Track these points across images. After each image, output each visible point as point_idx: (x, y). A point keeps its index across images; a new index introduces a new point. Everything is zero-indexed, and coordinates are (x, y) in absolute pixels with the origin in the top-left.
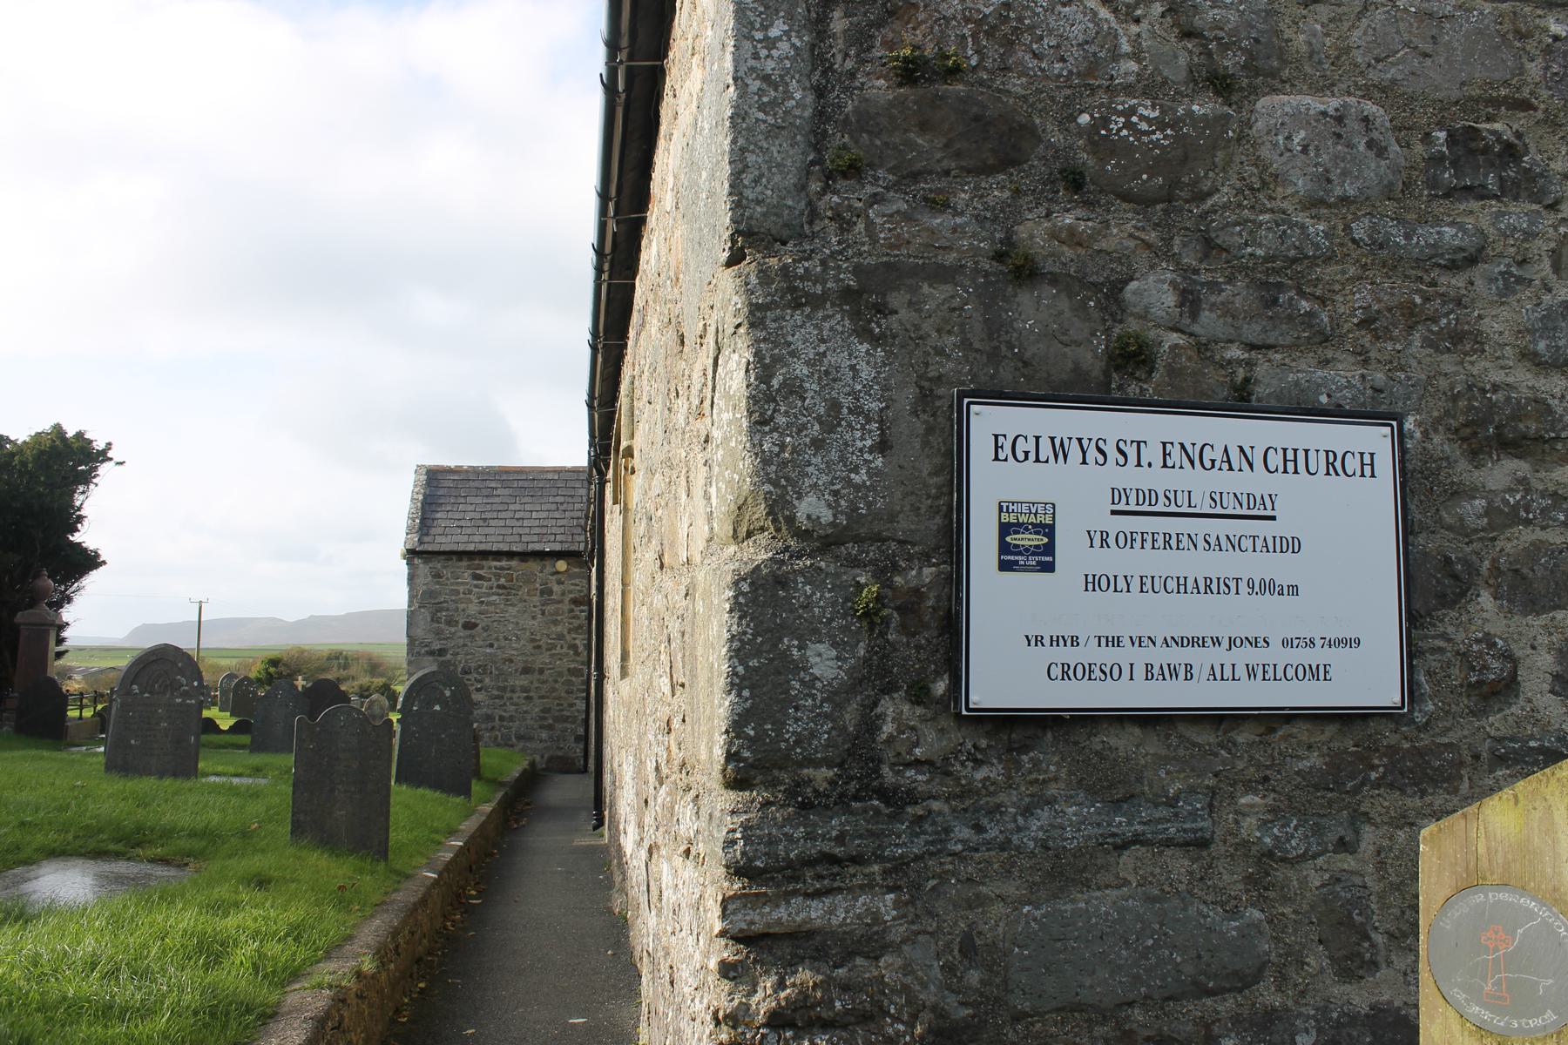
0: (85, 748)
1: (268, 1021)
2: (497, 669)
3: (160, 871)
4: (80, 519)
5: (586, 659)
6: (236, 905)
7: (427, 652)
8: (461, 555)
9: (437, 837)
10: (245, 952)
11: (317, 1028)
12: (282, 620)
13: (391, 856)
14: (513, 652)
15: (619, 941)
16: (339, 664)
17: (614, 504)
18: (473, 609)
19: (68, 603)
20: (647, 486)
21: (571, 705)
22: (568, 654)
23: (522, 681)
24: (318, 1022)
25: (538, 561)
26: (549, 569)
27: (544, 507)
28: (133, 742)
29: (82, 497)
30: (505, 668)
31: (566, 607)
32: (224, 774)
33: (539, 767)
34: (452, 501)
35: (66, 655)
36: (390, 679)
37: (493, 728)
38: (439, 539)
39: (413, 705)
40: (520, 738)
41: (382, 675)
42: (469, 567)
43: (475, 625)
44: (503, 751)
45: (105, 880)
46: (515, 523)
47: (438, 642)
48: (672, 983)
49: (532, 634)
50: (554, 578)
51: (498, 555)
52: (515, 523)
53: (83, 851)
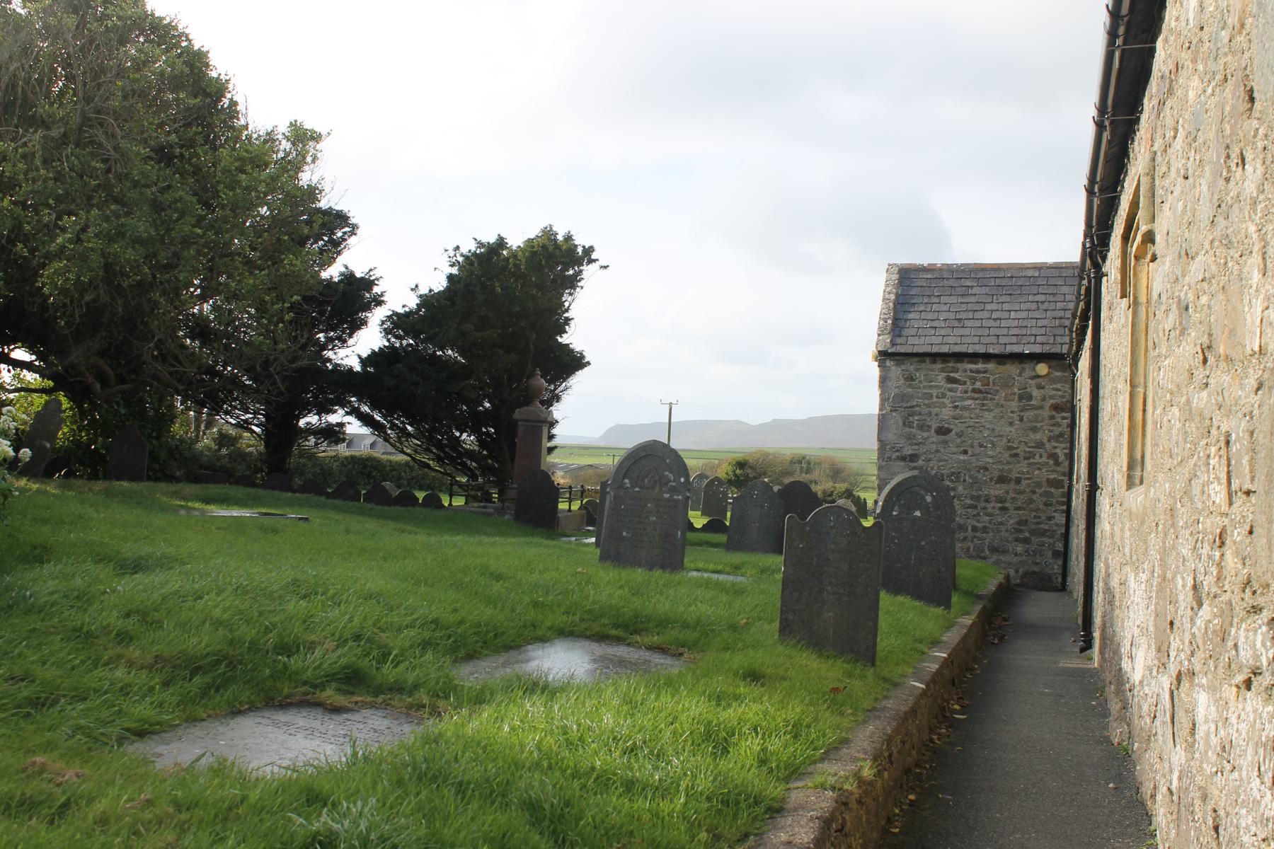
0: (574, 539)
1: (775, 815)
2: (971, 477)
3: (657, 659)
4: (568, 320)
5: (1067, 470)
6: (736, 697)
7: (898, 457)
8: (944, 357)
9: (921, 647)
10: (750, 746)
11: (823, 828)
12: (744, 423)
13: (878, 663)
14: (988, 460)
15: (1121, 774)
16: (802, 468)
17: (1122, 297)
18: (947, 413)
19: (557, 402)
20: (1179, 273)
21: (1050, 518)
22: (1047, 464)
23: (998, 491)
24: (824, 822)
25: (1017, 363)
26: (1028, 373)
27: (1023, 306)
28: (624, 534)
29: (570, 299)
30: (980, 476)
31: (1046, 413)
32: (706, 571)
33: (1013, 582)
34: (925, 301)
35: (556, 451)
36: (851, 484)
37: (965, 539)
38: (911, 341)
39: (893, 510)
40: (994, 550)
41: (843, 481)
42: (942, 370)
43: (949, 431)
44: (978, 563)
45: (602, 660)
46: (991, 323)
47: (909, 447)
48: (1216, 829)
49: (1009, 442)
50: (1033, 382)
51: (974, 357)
52: (991, 323)
53: (588, 633)
